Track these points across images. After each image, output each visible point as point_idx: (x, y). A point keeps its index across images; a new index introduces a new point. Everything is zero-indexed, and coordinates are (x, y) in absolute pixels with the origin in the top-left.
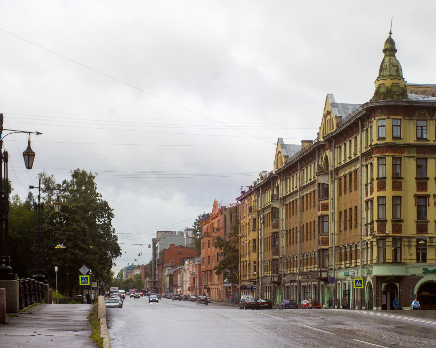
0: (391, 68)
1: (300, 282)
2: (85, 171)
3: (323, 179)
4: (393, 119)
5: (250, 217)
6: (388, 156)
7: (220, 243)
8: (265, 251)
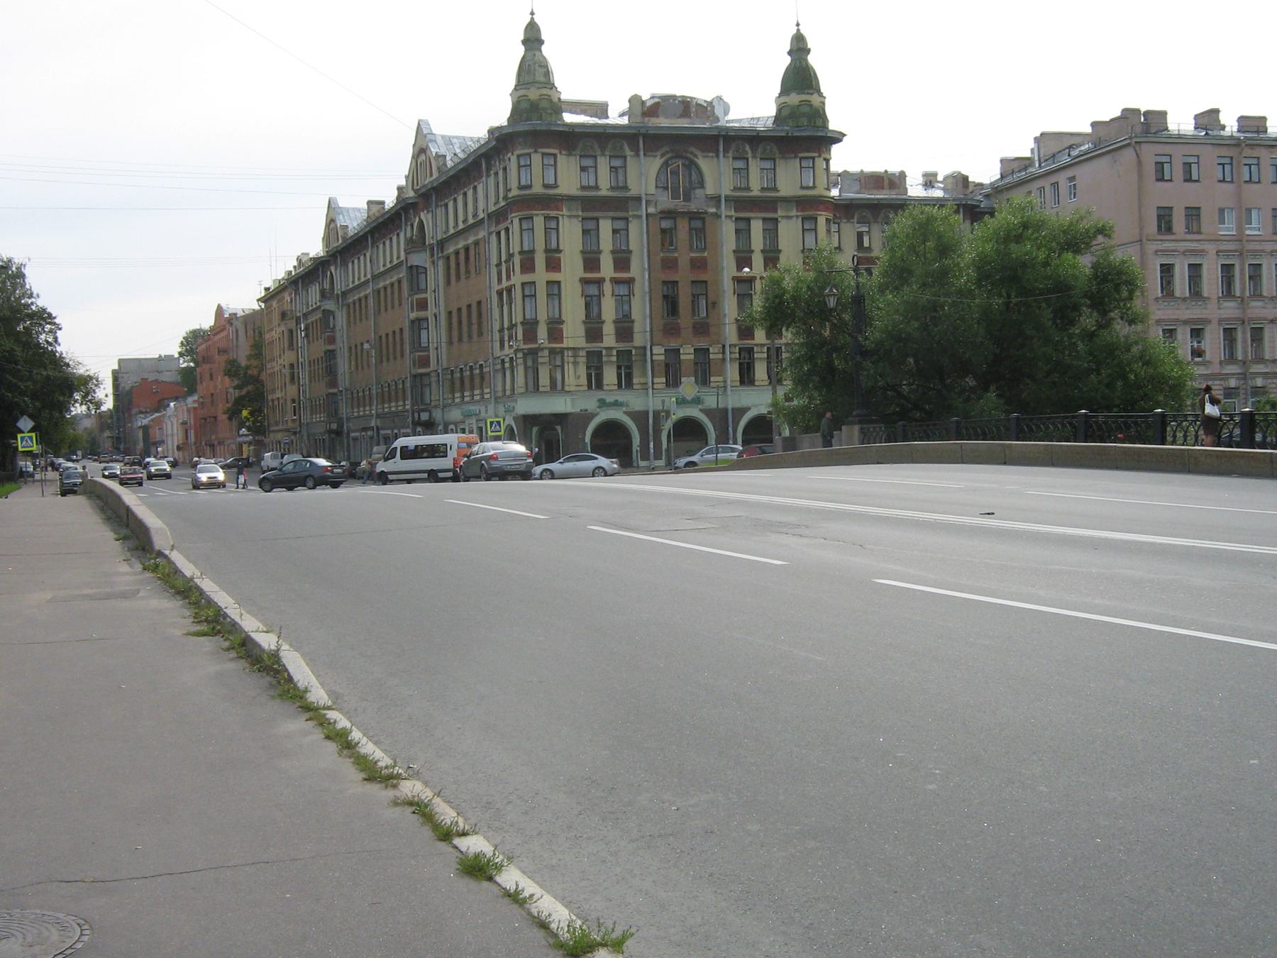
0: (533, 71)
1: (378, 429)
2: (26, 271)
3: (329, 305)
4: (543, 154)
5: (283, 328)
6: (606, 218)
7: (232, 370)
8: (310, 381)
